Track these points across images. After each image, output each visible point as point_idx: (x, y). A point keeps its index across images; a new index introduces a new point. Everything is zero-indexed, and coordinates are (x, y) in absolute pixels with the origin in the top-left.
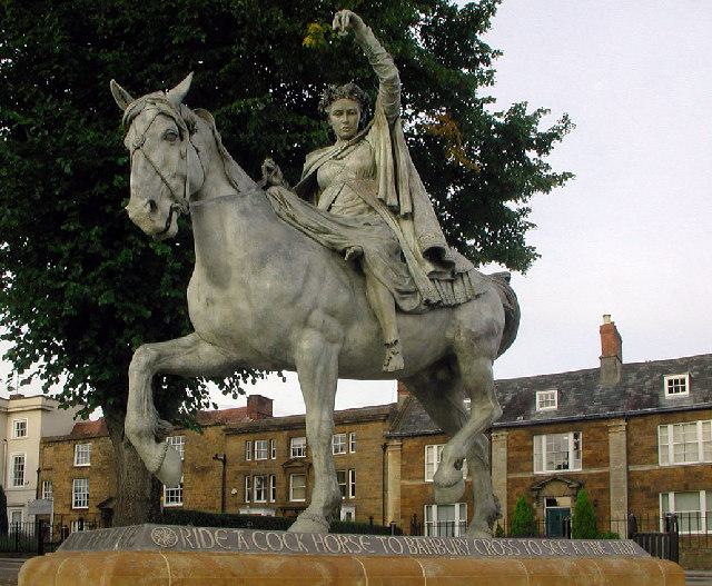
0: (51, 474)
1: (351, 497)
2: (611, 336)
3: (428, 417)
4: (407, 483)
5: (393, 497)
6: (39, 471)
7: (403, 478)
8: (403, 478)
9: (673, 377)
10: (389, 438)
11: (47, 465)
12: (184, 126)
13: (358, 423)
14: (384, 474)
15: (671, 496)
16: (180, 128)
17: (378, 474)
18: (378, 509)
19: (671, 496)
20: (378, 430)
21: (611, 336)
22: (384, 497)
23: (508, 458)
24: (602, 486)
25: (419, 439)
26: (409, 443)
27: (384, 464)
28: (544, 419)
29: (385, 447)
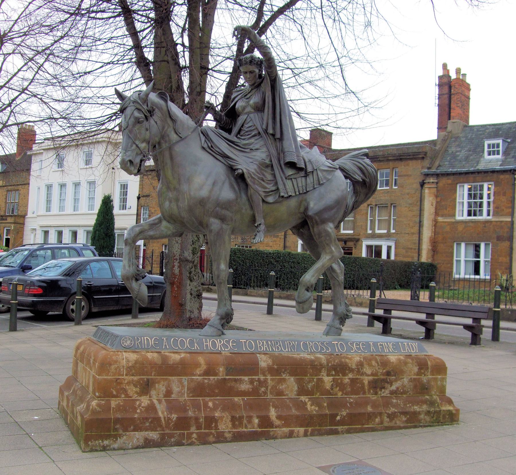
0: (148, 200)
1: (393, 231)
2: (452, 94)
3: (16, 136)
4: (440, 219)
5: (427, 233)
6: (139, 198)
7: (468, 199)
8: (468, 199)
9: (492, 142)
10: (427, 175)
11: (146, 192)
12: (148, 115)
13: (401, 160)
14: (421, 210)
15: (463, 245)
16: (145, 116)
17: (416, 208)
18: (415, 243)
19: (463, 245)
20: (415, 169)
21: (452, 94)
22: (420, 233)
23: (91, 316)
24: (225, 426)
25: (452, 177)
26: (444, 181)
27: (421, 200)
28: (490, 167)
29: (422, 184)
